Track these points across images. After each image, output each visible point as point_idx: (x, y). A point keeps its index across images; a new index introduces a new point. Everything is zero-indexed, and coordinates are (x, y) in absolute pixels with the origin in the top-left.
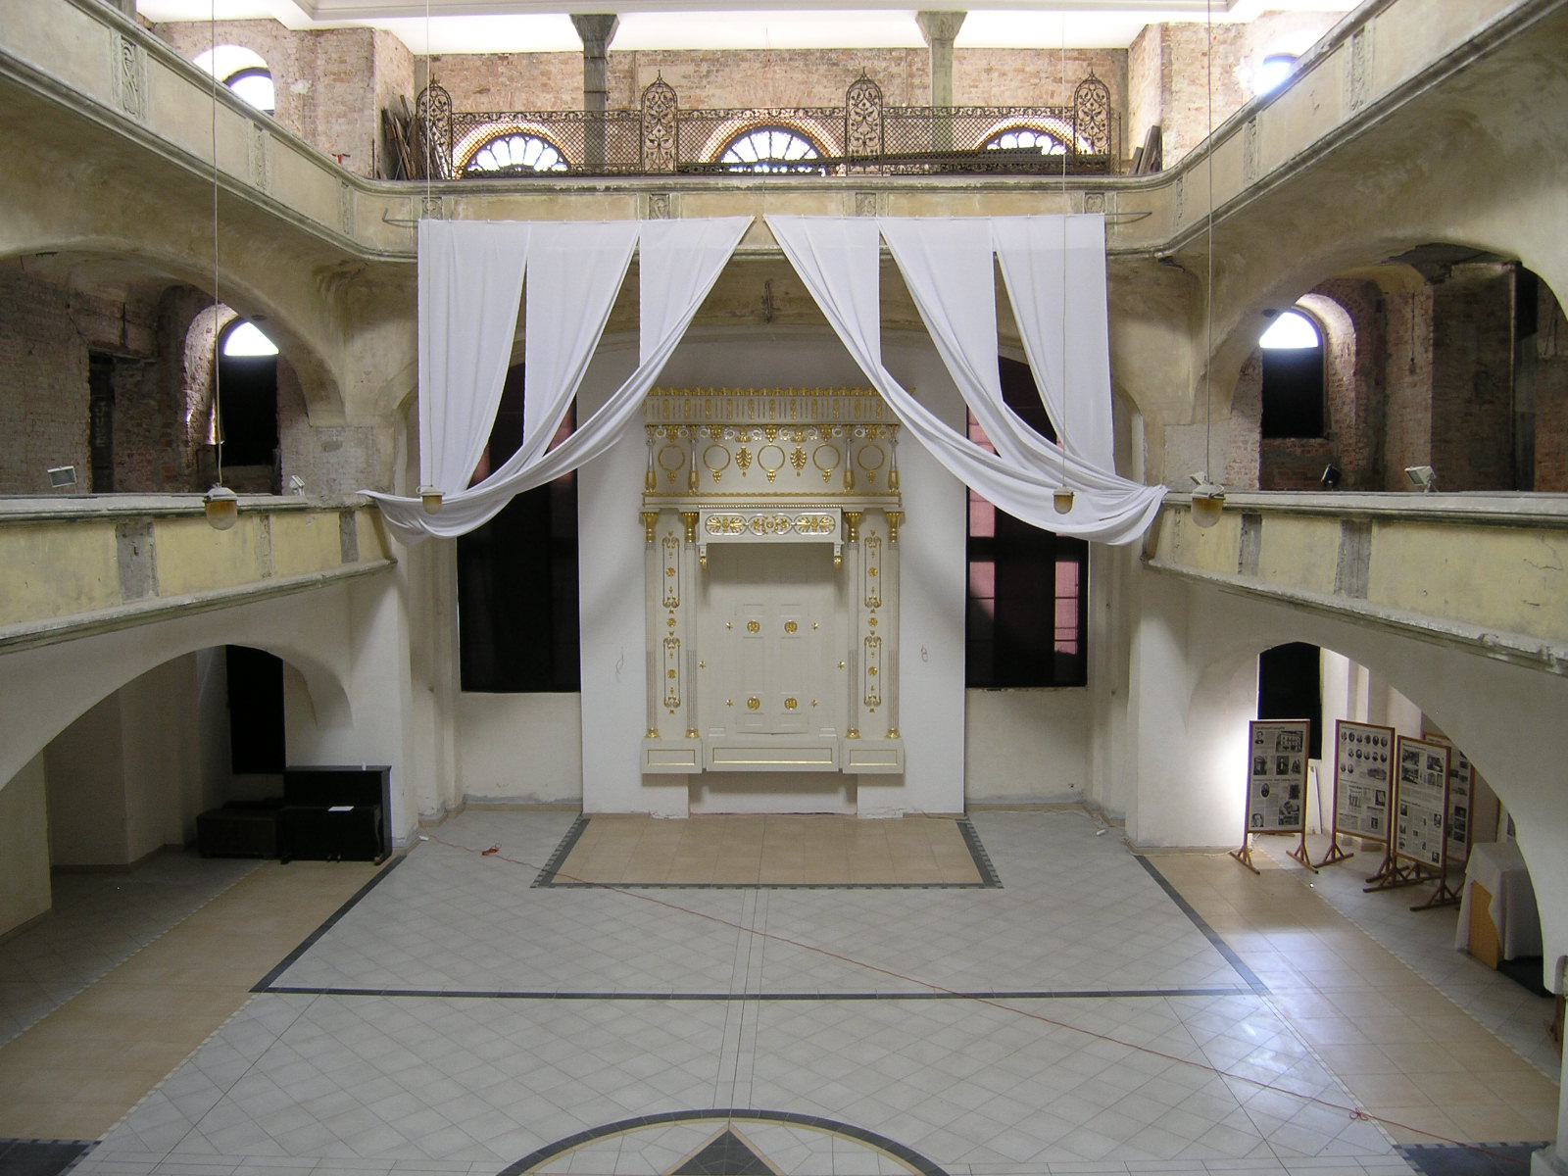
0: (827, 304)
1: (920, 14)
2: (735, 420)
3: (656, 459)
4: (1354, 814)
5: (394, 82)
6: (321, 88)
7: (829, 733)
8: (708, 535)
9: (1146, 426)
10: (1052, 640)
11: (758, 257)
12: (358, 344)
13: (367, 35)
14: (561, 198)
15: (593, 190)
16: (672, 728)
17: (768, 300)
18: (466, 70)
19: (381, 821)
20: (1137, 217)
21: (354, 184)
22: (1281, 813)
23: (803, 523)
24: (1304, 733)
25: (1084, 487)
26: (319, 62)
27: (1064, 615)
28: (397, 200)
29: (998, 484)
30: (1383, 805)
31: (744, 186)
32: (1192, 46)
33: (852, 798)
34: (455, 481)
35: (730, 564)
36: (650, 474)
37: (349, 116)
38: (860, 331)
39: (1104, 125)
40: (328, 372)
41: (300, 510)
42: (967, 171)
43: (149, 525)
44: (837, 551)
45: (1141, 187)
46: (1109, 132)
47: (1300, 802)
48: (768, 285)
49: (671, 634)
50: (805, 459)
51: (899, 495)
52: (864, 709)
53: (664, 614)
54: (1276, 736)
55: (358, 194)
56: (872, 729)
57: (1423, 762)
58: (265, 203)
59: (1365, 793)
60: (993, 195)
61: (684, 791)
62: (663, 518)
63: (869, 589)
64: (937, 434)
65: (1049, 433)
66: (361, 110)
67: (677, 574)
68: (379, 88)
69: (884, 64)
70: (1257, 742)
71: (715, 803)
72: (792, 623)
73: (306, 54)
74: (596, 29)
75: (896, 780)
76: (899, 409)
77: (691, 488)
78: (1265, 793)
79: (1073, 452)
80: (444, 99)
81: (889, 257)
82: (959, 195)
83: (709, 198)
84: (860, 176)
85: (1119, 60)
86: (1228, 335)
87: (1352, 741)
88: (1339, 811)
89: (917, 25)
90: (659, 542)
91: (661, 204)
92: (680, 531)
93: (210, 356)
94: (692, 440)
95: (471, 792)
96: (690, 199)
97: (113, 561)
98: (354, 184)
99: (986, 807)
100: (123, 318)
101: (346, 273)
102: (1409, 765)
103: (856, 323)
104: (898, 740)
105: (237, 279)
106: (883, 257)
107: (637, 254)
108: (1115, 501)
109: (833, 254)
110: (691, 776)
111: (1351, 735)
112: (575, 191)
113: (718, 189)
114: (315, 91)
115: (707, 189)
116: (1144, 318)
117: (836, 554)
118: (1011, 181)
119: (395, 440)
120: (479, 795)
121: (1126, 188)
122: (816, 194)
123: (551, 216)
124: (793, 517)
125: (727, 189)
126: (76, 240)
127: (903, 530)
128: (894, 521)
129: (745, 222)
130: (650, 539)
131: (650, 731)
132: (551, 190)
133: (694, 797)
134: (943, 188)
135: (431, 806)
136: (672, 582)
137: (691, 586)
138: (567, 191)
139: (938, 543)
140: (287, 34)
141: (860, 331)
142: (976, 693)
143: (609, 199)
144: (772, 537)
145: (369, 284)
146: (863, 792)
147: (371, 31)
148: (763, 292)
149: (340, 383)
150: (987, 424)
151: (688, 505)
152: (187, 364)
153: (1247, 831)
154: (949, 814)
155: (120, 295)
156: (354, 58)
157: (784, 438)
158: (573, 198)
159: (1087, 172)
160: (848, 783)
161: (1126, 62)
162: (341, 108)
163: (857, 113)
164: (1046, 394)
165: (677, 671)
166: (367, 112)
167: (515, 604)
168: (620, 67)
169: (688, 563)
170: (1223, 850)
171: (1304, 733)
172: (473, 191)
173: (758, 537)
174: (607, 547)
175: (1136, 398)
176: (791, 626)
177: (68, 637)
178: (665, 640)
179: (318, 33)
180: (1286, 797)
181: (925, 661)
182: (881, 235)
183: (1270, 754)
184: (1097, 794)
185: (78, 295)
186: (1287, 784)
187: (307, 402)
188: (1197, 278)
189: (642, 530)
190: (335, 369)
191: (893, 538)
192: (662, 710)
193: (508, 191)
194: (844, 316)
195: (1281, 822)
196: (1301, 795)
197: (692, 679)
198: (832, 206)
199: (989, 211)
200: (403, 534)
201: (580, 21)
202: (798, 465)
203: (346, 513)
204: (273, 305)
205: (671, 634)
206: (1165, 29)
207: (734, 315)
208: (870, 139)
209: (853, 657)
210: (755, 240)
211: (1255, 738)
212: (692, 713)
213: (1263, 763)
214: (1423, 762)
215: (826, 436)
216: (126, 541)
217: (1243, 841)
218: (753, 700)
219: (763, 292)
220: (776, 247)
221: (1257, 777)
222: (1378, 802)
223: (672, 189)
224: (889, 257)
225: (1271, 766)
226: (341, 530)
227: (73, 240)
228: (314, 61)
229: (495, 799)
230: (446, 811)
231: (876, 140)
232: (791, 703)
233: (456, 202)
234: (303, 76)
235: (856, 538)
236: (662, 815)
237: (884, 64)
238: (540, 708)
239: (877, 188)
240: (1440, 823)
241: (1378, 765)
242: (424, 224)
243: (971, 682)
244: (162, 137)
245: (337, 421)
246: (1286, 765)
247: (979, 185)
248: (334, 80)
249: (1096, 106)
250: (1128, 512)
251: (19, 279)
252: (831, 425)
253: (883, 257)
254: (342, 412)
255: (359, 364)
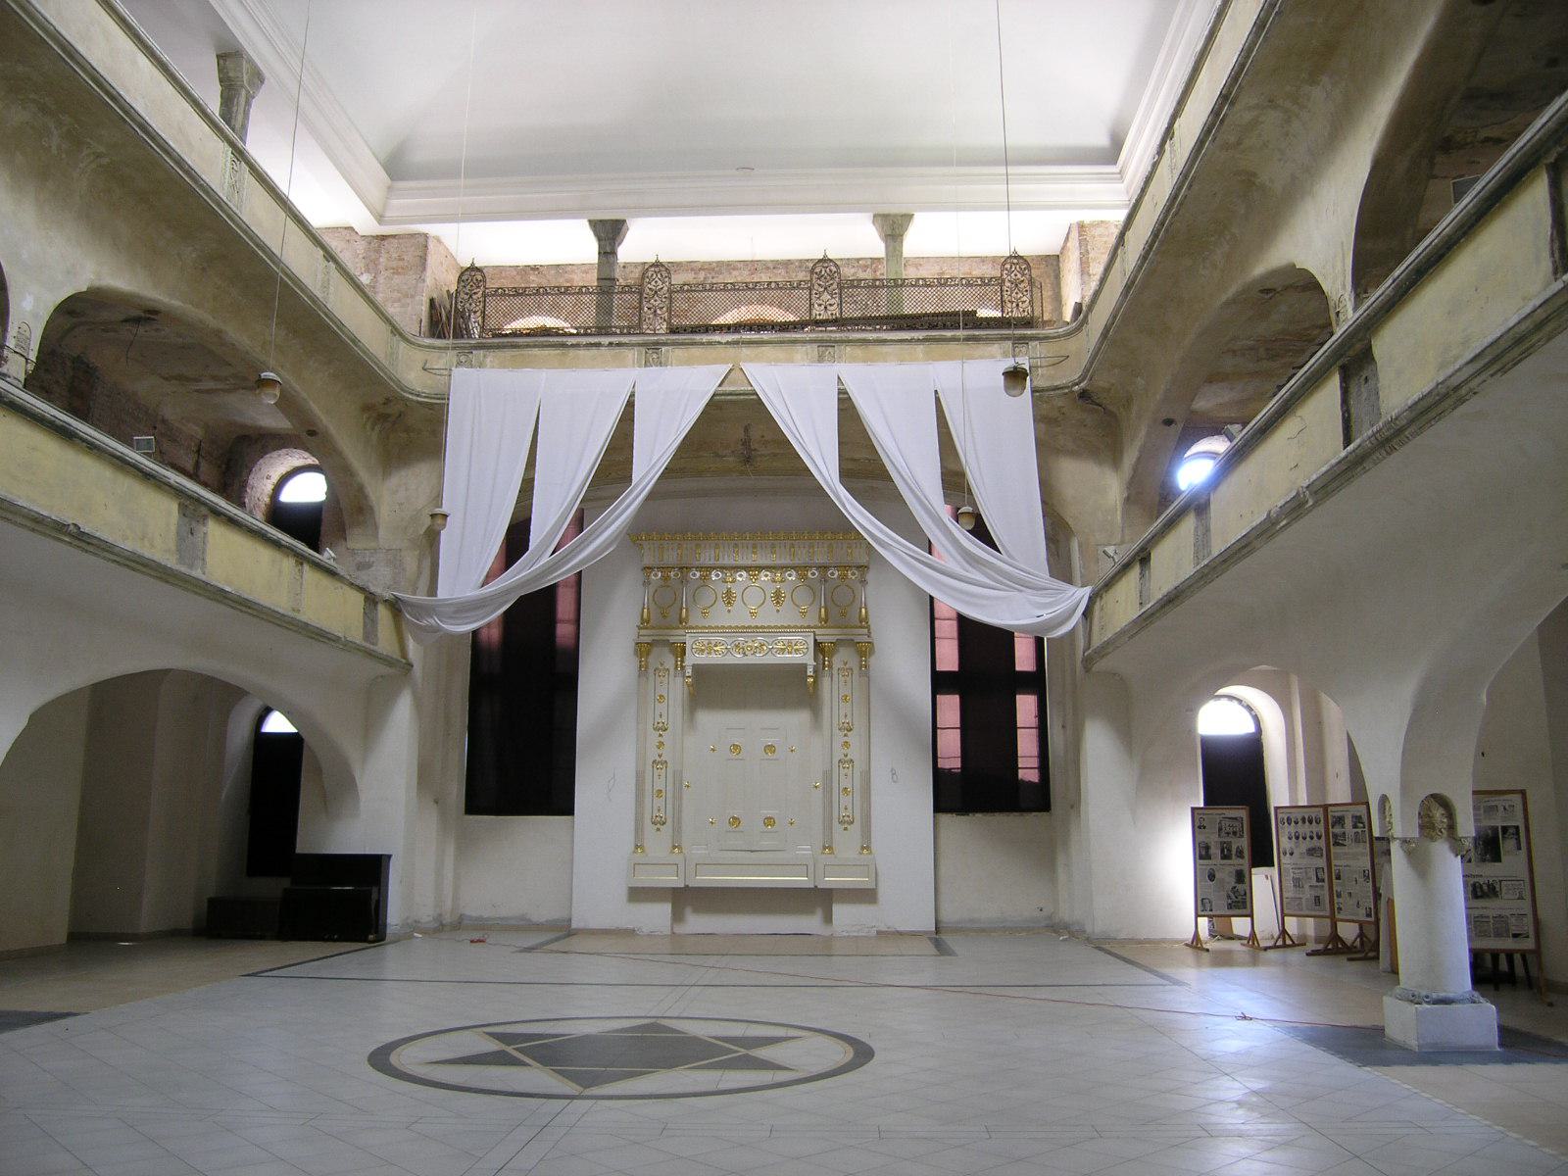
0: (789, 429)
1: (874, 216)
2: (721, 562)
3: (651, 598)
4: (1298, 896)
5: (441, 278)
6: (381, 279)
7: (804, 851)
8: (692, 658)
9: (1080, 546)
10: (1016, 768)
11: (735, 397)
12: (395, 480)
13: (422, 240)
14: (572, 352)
15: (598, 345)
16: (658, 845)
17: (746, 443)
18: (504, 278)
19: (378, 901)
20: (1056, 360)
21: (401, 334)
22: (1229, 897)
23: (780, 646)
24: (1245, 819)
25: (1022, 588)
26: (381, 260)
27: (1027, 745)
28: (436, 354)
29: (938, 581)
30: (1323, 881)
31: (724, 341)
32: (1104, 239)
33: (828, 918)
34: (469, 582)
35: (717, 688)
36: (645, 610)
37: (403, 301)
38: (822, 456)
39: (1026, 291)
40: (366, 497)
41: (331, 573)
42: (911, 328)
43: (205, 517)
44: (810, 671)
45: (1059, 337)
46: (1031, 296)
47: (1246, 886)
48: (746, 430)
49: (660, 756)
50: (784, 597)
51: (868, 628)
52: (837, 828)
53: (653, 738)
54: (1218, 821)
55: (403, 345)
56: (847, 843)
57: (1349, 823)
58: (326, 315)
59: (1306, 873)
60: (934, 346)
61: (666, 908)
62: (655, 650)
63: (842, 714)
64: (890, 542)
65: (992, 544)
66: (412, 296)
67: (666, 701)
68: (429, 281)
69: (853, 271)
70: (1200, 827)
71: (697, 923)
72: (772, 746)
73: (372, 254)
74: (609, 233)
75: (866, 896)
76: (853, 518)
77: (681, 623)
78: (1212, 877)
79: (1010, 556)
80: (479, 278)
81: (846, 396)
82: (905, 347)
83: (695, 351)
84: (819, 334)
85: (1052, 264)
86: (1140, 451)
87: (1289, 824)
88: (1285, 895)
89: (874, 228)
90: (651, 671)
91: (655, 356)
92: (669, 661)
93: (267, 500)
94: (684, 581)
95: (468, 912)
96: (679, 352)
97: (173, 528)
98: (401, 334)
99: (959, 930)
100: (198, 451)
101: (389, 416)
102: (1337, 830)
103: (819, 451)
104: (870, 856)
105: (298, 387)
106: (841, 396)
107: (632, 395)
108: (1048, 600)
109: (798, 394)
110: (675, 889)
111: (1289, 820)
112: (584, 346)
113: (703, 344)
114: (376, 282)
115: (694, 344)
116: (1073, 454)
117: (809, 674)
118: (949, 334)
119: (420, 561)
120: (474, 914)
121: (1046, 338)
122: (785, 347)
123: (562, 365)
124: (770, 640)
125: (710, 343)
126: (176, 303)
127: (872, 661)
128: (864, 651)
129: (723, 369)
130: (643, 670)
131: (637, 847)
132: (563, 345)
133: (677, 916)
134: (891, 341)
135: (426, 914)
136: (661, 708)
137: (679, 711)
138: (576, 346)
139: (905, 664)
140: (357, 238)
141: (822, 456)
142: (945, 818)
143: (613, 352)
144: (750, 660)
145: (407, 430)
146: (840, 911)
147: (426, 236)
148: (741, 434)
149: (376, 509)
150: (938, 540)
151: (676, 637)
152: (246, 500)
153: (1197, 916)
154: (919, 932)
155: (198, 432)
156: (410, 257)
157: (765, 577)
158: (582, 352)
159: (1015, 328)
160: (820, 899)
161: (1058, 265)
162: (396, 295)
163: (819, 285)
164: (991, 521)
165: (664, 791)
166: (417, 298)
167: (518, 730)
168: (632, 275)
169: (676, 689)
170: (1177, 941)
171: (1245, 819)
172: (499, 347)
173: (737, 658)
174: (605, 679)
175: (1071, 522)
176: (770, 748)
177: (133, 565)
178: (654, 762)
179: (383, 238)
180: (1232, 881)
181: (894, 782)
182: (839, 378)
183: (1214, 839)
184: (1065, 913)
185: (164, 421)
186: (1233, 869)
187: (347, 527)
188: (1116, 416)
189: (635, 661)
190: (373, 497)
191: (864, 668)
192: (649, 828)
193: (528, 346)
194: (806, 439)
195: (1230, 906)
196: (1247, 880)
197: (678, 797)
198: (798, 356)
199: (930, 358)
200: (421, 632)
201: (597, 226)
202: (778, 603)
203: (371, 599)
204: (324, 421)
205: (660, 756)
206: (1081, 227)
207: (717, 455)
208: (831, 305)
209: (828, 777)
210: (732, 384)
211: (1197, 825)
212: (677, 830)
213: (1207, 848)
214: (1349, 823)
215: (802, 577)
216: (186, 520)
217: (1194, 925)
218: (734, 818)
219: (741, 434)
220: (750, 388)
221: (1202, 861)
222: (1318, 880)
223: (665, 344)
224: (846, 396)
225: (1215, 851)
226: (365, 613)
227: (173, 302)
228: (378, 259)
229: (487, 919)
230: (442, 925)
231: (835, 306)
232: (769, 821)
233: (485, 356)
234: (368, 270)
235: (830, 667)
236: (646, 930)
237: (853, 271)
238: (533, 831)
239: (836, 342)
240: (1368, 877)
241: (1316, 843)
242: (457, 372)
243: (939, 807)
244: (252, 228)
245: (373, 544)
246: (1229, 850)
247: (921, 338)
248: (394, 273)
249: (1019, 276)
250: (1061, 608)
251: (119, 394)
252: (806, 568)
253: (841, 396)
254: (376, 536)
255: (394, 496)
